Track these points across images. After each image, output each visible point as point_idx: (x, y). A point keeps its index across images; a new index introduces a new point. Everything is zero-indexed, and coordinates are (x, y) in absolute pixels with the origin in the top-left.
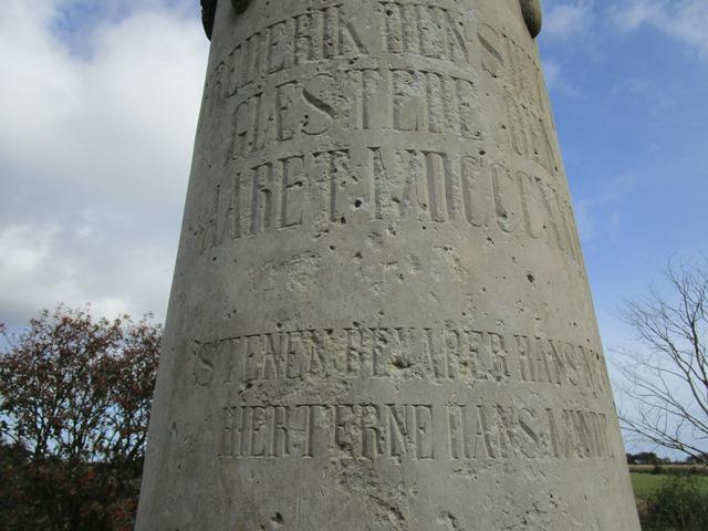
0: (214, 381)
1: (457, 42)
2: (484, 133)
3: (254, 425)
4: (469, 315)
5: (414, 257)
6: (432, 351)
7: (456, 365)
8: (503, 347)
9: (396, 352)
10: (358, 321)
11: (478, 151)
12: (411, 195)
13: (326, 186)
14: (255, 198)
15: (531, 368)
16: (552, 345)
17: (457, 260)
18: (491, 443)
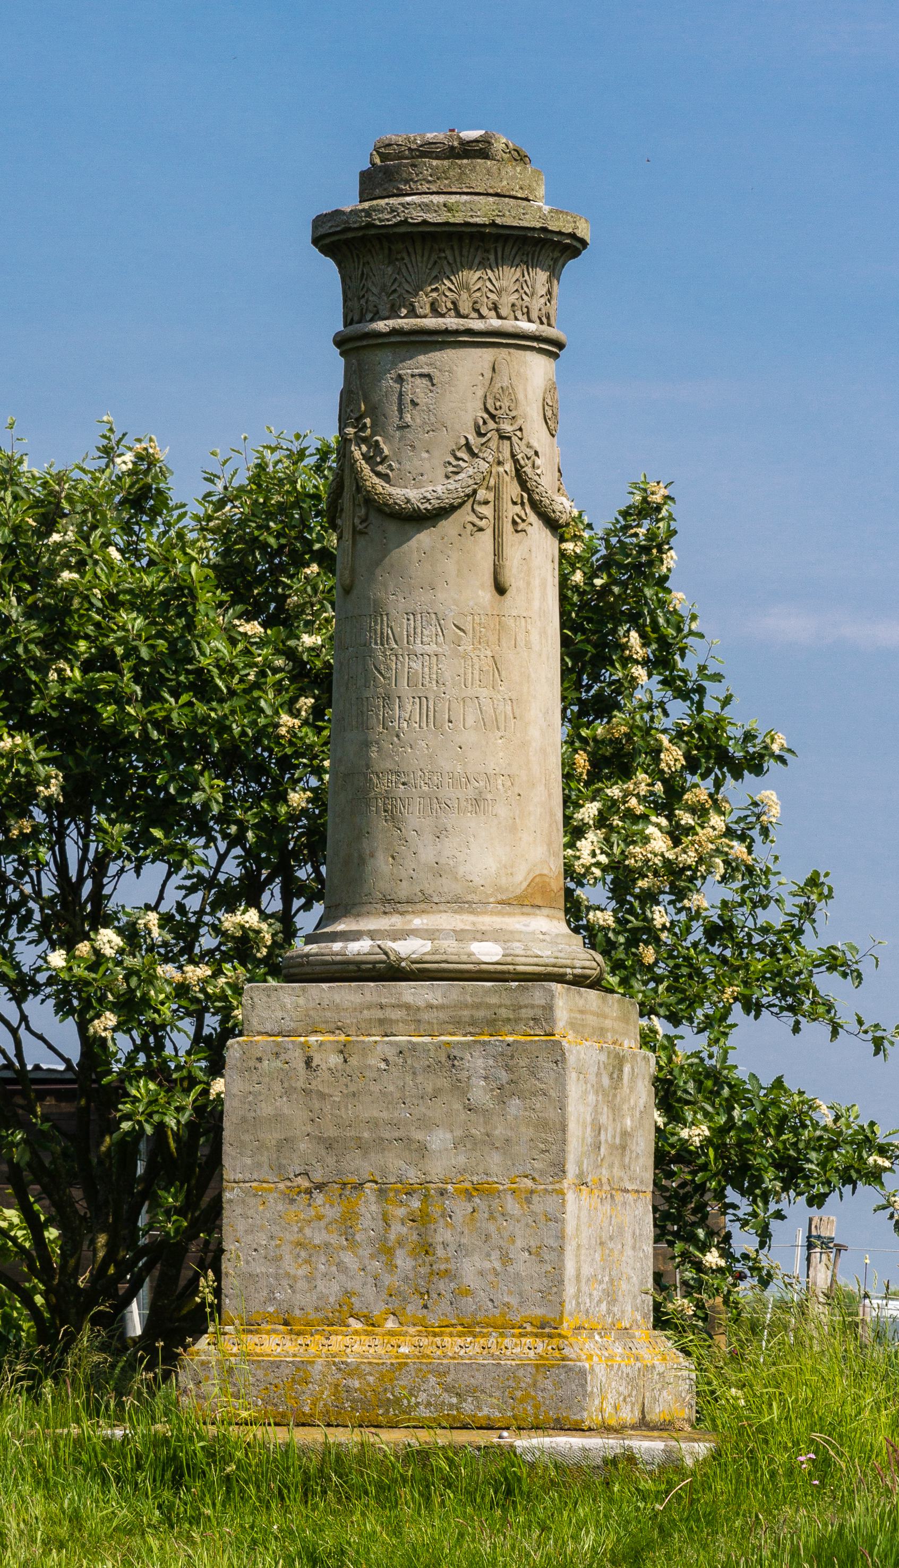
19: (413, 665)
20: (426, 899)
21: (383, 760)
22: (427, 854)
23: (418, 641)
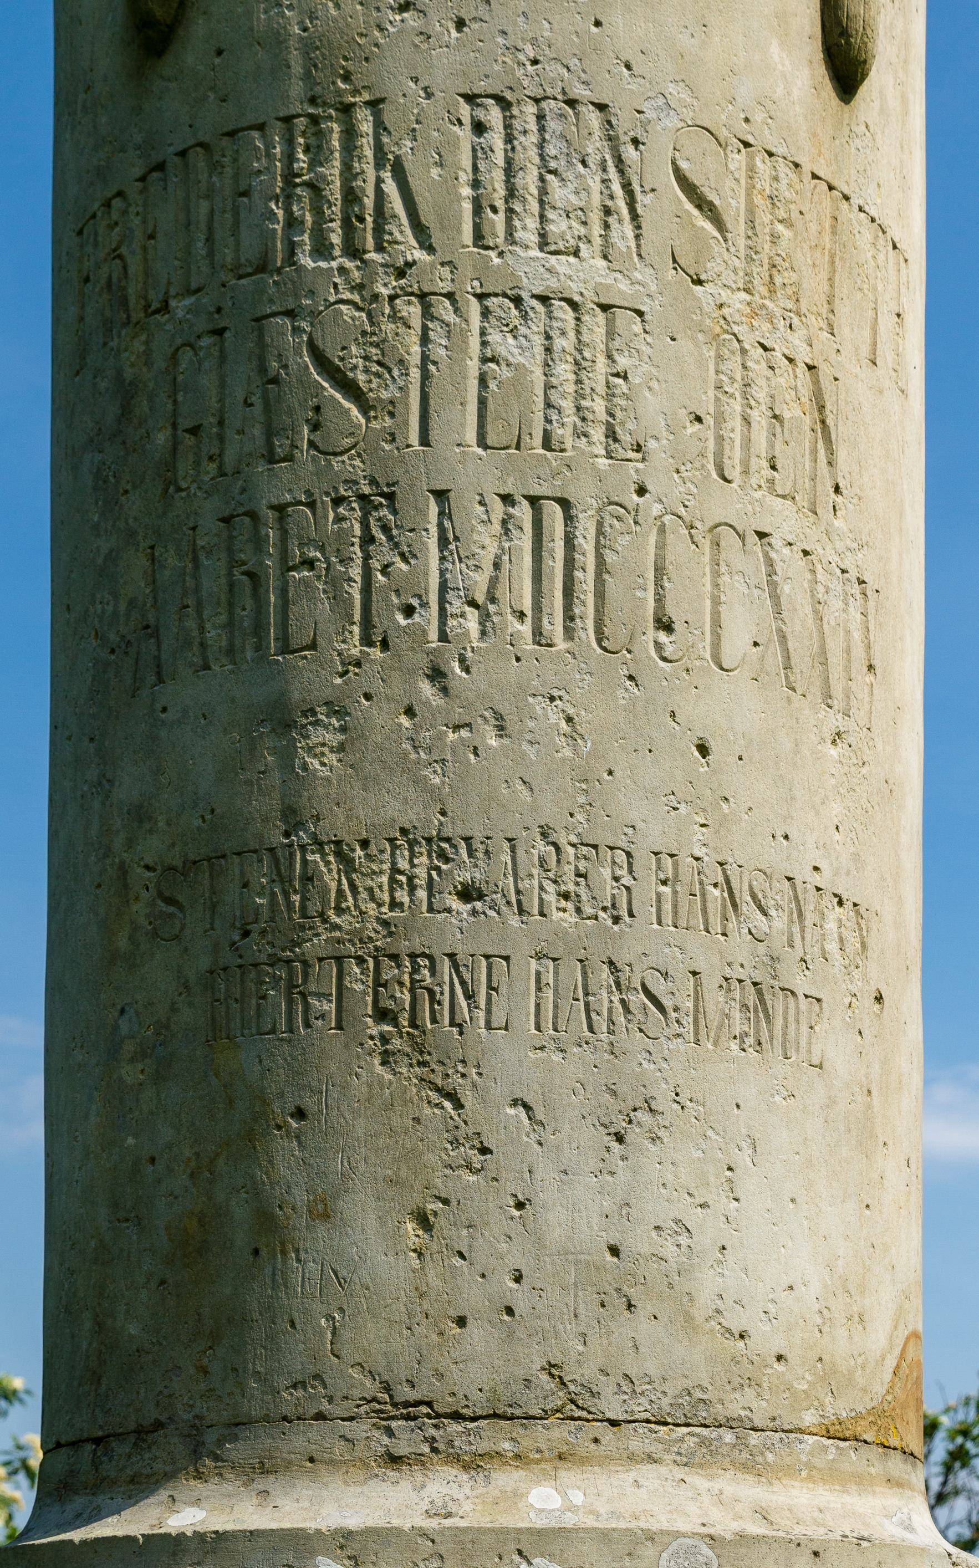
0: (187, 932)
1: (621, 204)
2: (652, 444)
3: (258, 990)
4: (580, 817)
5: (499, 716)
6: (516, 876)
7: (551, 898)
8: (631, 871)
9: (463, 876)
10: (407, 826)
11: (633, 487)
12: (498, 595)
13: (356, 572)
14: (231, 586)
15: (675, 906)
16: (724, 871)
17: (569, 720)
18: (593, 1015)
19: (502, 343)
20: (576, 1407)
21: (368, 782)
22: (574, 1212)
23: (528, 232)
